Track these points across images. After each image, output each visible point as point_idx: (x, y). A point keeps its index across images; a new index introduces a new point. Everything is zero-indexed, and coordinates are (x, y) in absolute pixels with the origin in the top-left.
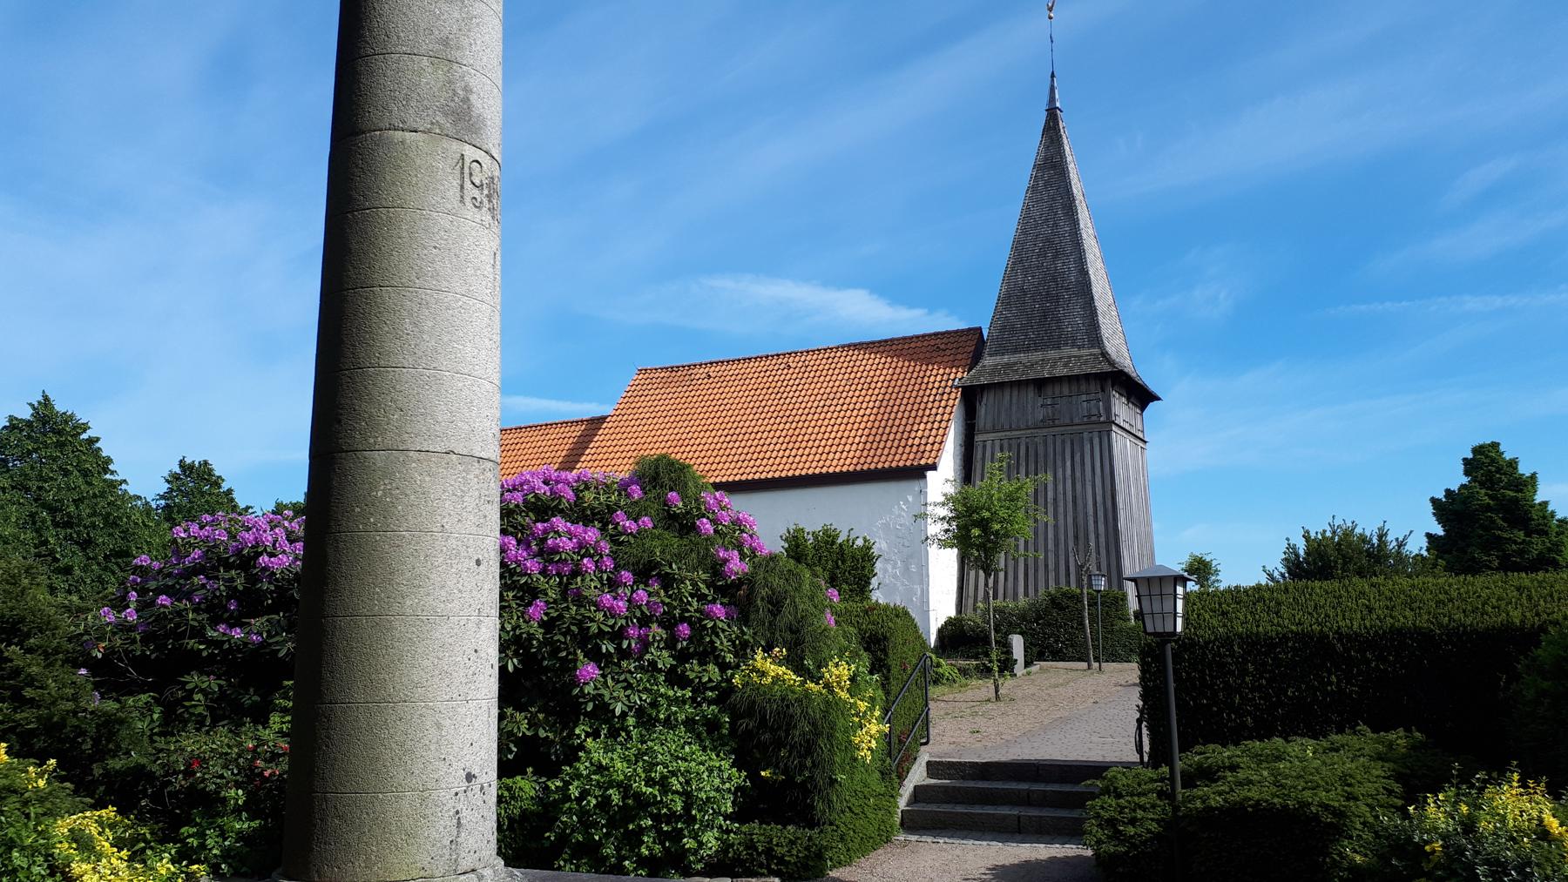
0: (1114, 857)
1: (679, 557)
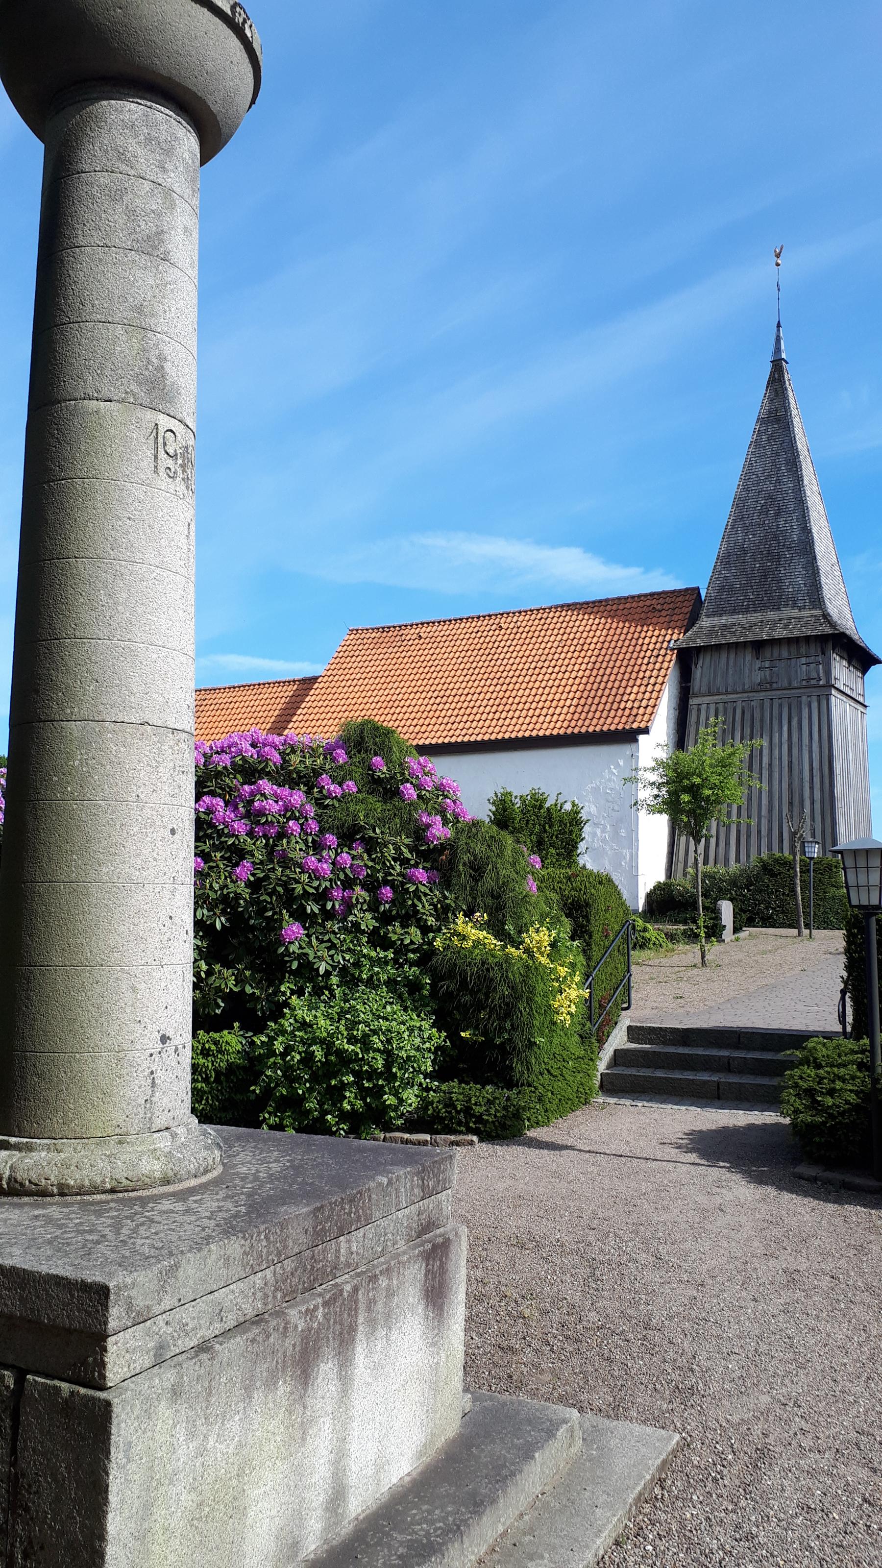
0: (811, 1127)
1: (382, 821)
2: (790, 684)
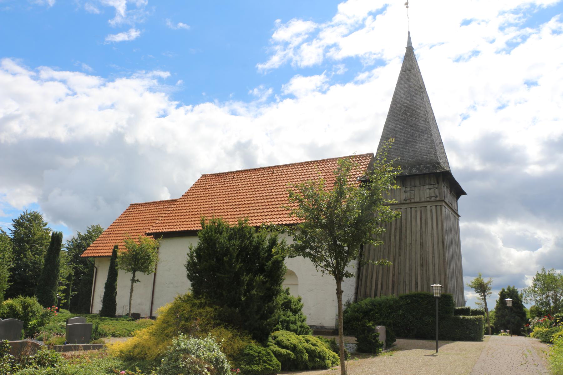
2: (420, 199)
